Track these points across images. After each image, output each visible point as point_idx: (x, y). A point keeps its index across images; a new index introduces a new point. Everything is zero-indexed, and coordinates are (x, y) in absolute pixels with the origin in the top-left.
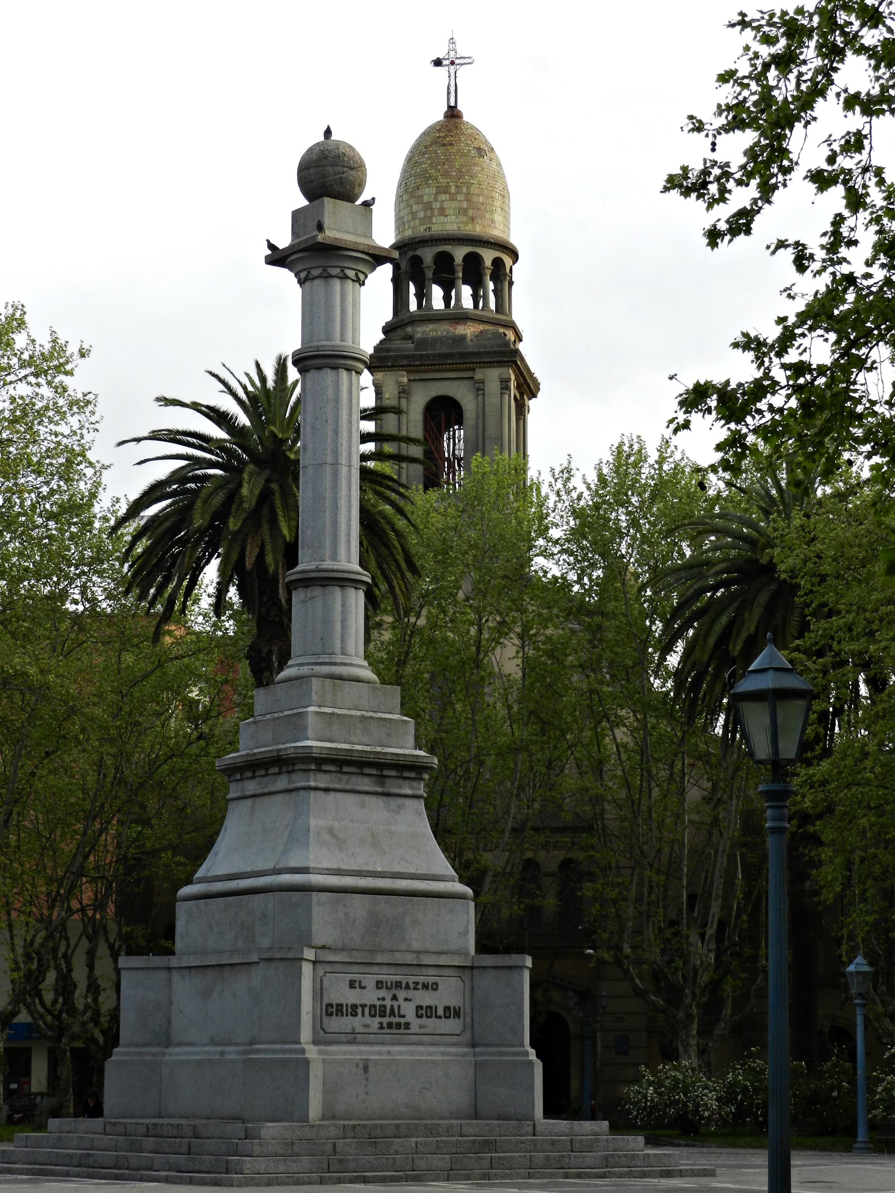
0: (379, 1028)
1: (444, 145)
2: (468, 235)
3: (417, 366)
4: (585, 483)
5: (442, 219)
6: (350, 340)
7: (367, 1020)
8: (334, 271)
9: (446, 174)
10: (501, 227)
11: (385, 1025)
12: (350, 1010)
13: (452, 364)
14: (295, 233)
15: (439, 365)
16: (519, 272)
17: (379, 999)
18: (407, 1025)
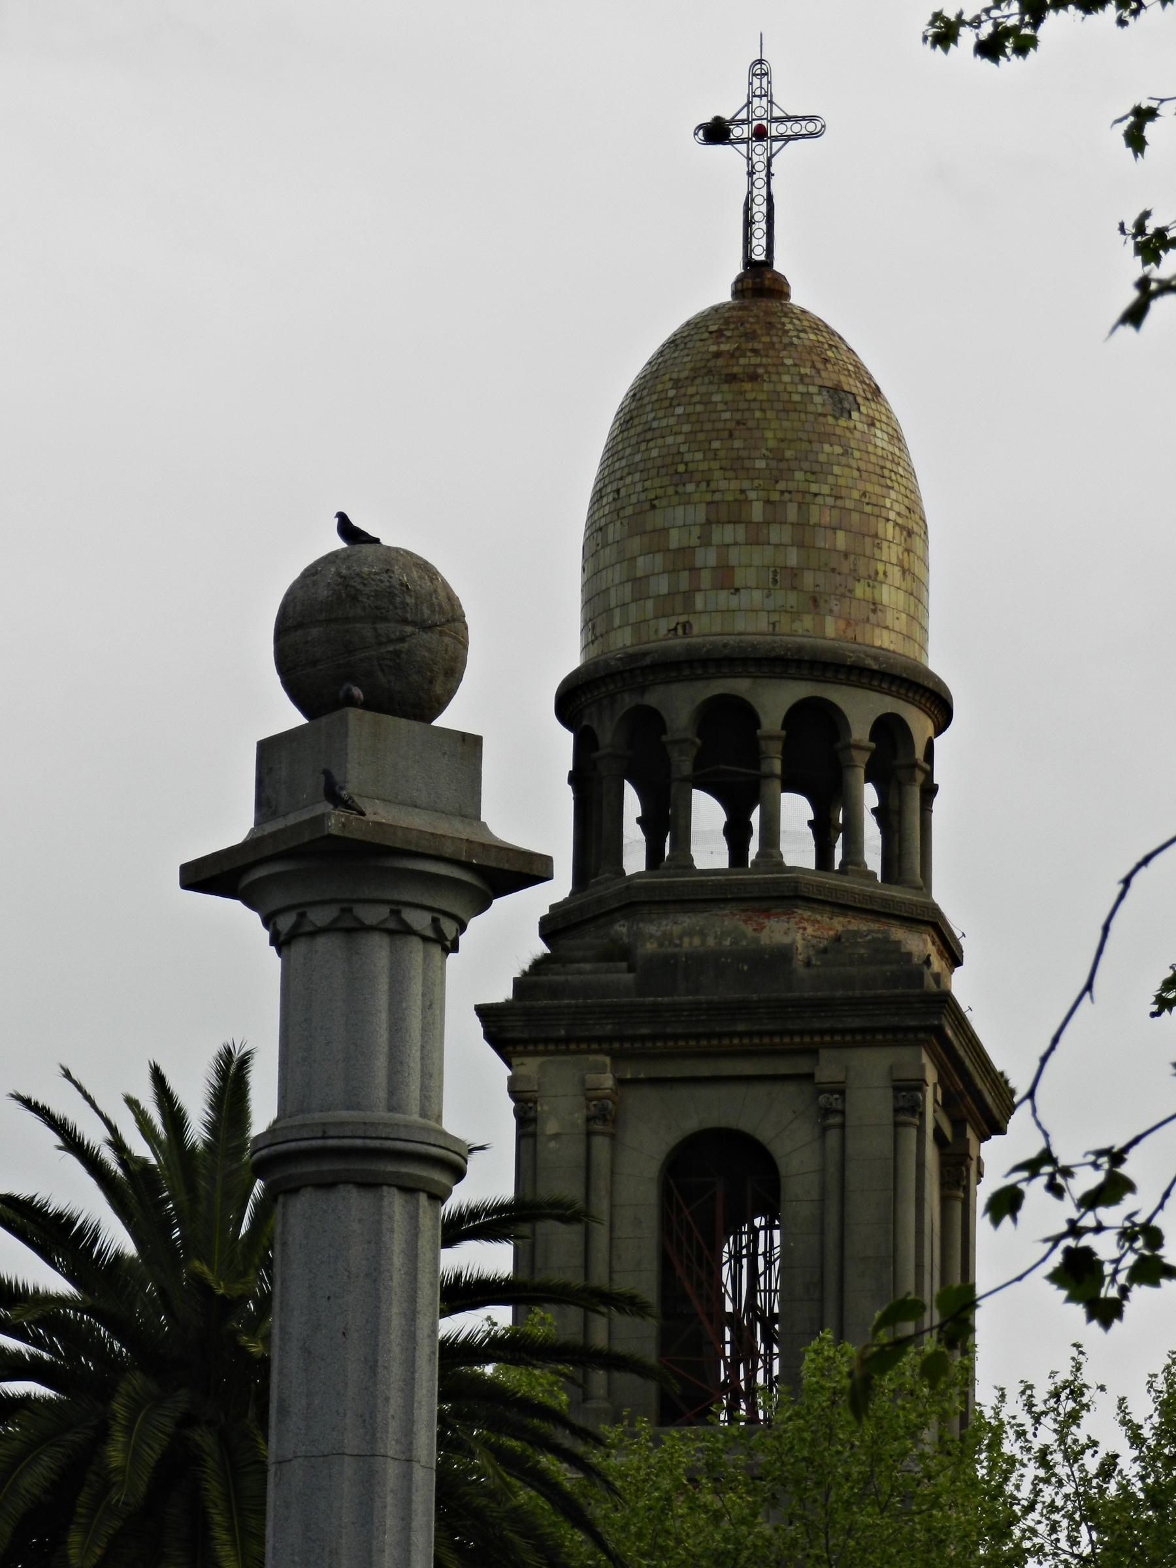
1: (732, 378)
2: (800, 648)
3: (644, 1038)
4: (1124, 1423)
5: (724, 598)
6: (414, 1105)
8: (372, 915)
9: (737, 466)
10: (901, 623)
13: (750, 1034)
14: (266, 803)
15: (709, 1036)
16: (951, 755)
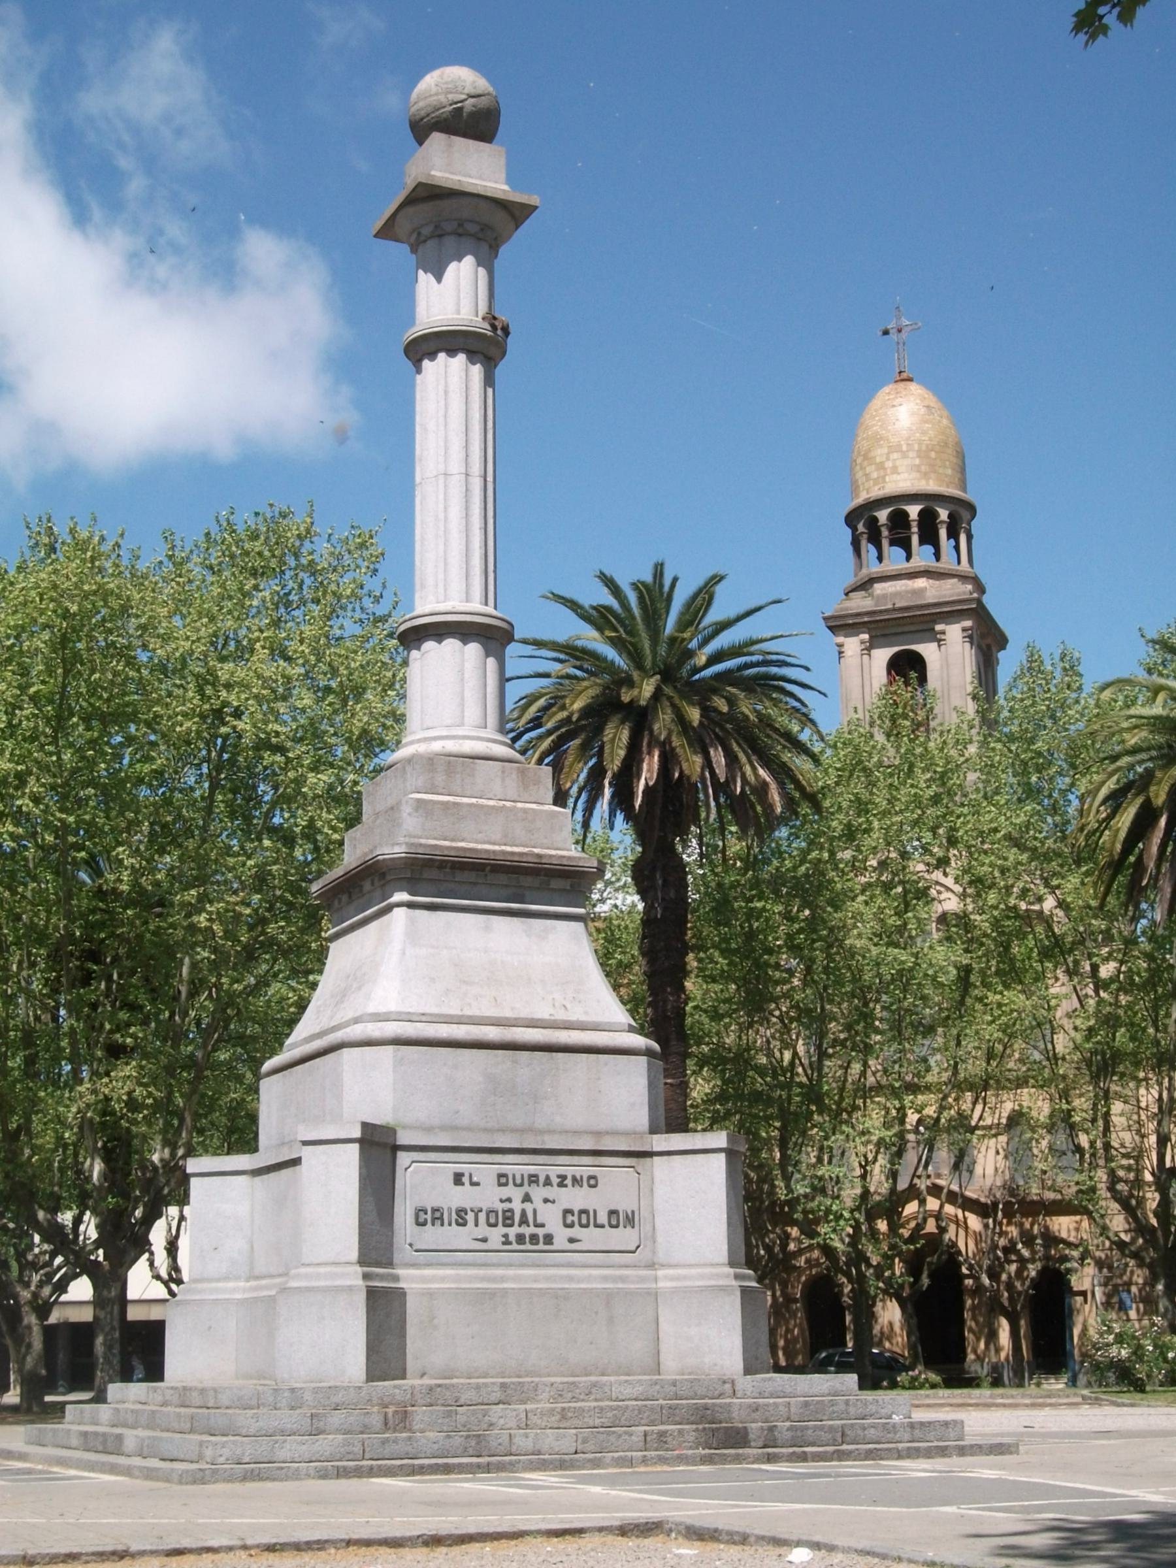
0: (504, 1243)
5: (895, 477)
7: (483, 1230)
11: (512, 1238)
12: (454, 1216)
17: (502, 1201)
18: (549, 1239)
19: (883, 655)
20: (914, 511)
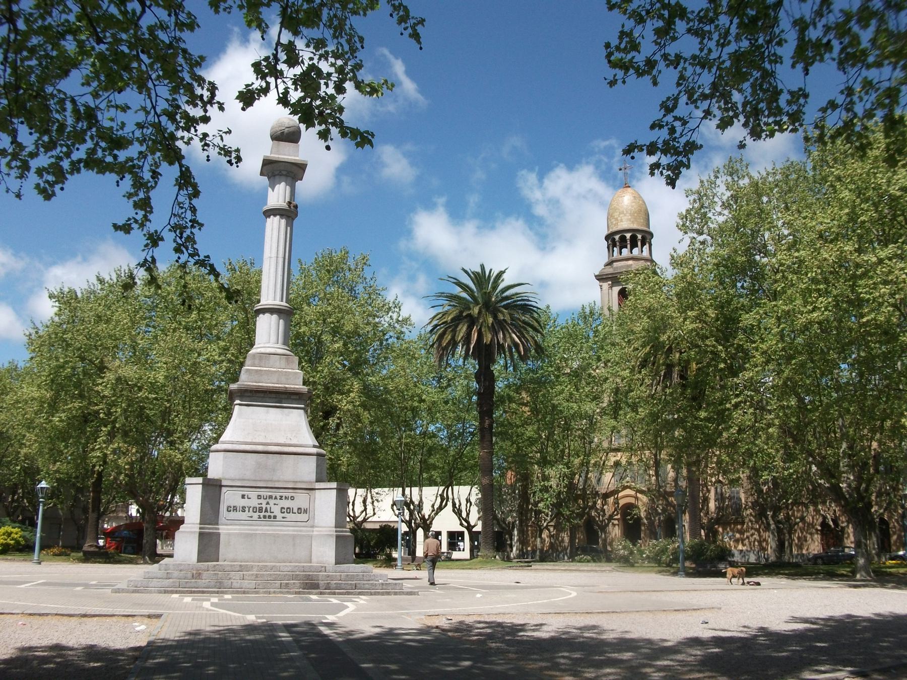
7: (251, 513)
18: (275, 517)
19: (616, 289)
20: (628, 235)
